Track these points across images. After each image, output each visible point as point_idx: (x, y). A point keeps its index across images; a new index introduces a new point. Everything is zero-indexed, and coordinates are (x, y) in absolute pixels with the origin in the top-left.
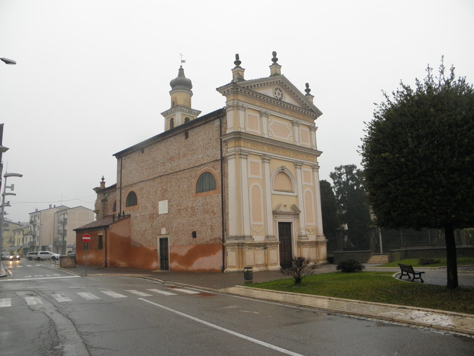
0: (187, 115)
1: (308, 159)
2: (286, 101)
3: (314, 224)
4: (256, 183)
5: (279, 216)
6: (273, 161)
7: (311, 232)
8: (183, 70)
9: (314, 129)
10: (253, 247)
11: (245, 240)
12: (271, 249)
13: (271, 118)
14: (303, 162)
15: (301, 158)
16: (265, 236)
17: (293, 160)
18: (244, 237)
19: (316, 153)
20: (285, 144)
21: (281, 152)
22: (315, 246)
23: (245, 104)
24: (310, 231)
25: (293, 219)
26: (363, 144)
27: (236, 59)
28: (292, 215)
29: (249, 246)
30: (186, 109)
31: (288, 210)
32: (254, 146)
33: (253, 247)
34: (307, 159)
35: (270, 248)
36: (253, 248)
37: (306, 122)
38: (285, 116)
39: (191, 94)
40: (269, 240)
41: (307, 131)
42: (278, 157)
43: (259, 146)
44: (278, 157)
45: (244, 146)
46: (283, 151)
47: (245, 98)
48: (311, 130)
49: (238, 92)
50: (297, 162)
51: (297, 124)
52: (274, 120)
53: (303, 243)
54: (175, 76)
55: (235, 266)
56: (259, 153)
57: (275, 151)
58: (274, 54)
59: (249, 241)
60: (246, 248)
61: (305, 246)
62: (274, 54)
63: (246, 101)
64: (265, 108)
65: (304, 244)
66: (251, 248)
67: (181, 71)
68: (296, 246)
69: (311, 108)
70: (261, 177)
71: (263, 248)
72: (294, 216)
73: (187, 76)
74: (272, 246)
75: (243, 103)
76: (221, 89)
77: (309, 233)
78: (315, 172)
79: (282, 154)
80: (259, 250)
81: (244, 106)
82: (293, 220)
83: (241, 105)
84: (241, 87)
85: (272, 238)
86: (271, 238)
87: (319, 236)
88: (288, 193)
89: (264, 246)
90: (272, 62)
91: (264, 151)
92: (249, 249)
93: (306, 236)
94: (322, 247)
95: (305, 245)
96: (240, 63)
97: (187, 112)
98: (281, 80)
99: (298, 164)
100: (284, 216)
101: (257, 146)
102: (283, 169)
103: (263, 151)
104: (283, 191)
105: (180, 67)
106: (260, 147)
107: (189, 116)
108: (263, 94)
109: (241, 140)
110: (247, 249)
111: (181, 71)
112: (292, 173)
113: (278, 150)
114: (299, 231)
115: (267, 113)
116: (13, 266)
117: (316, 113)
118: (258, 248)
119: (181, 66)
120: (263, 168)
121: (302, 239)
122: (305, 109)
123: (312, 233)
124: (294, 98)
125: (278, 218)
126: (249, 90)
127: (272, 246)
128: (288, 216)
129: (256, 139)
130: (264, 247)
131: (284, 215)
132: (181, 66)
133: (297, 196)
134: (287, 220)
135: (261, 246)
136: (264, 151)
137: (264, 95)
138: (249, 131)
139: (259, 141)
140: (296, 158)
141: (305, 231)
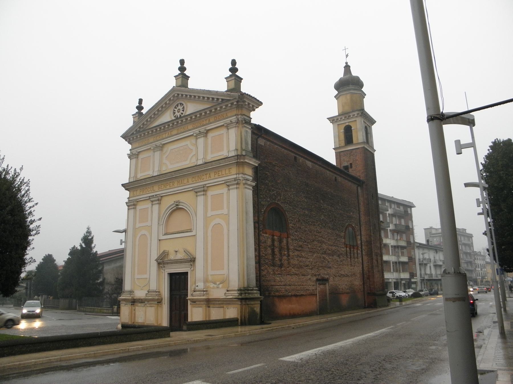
0: (346, 123)
3: (225, 272)
4: (217, 221)
7: (219, 284)
8: (350, 67)
10: (129, 303)
20: (173, 173)
25: (189, 267)
26: (29, 184)
27: (139, 104)
28: (186, 263)
30: (340, 117)
31: (180, 256)
35: (147, 305)
38: (179, 135)
39: (363, 95)
42: (185, 189)
43: (149, 189)
44: (185, 189)
45: (170, 188)
51: (202, 134)
54: (340, 74)
64: (157, 141)
67: (347, 68)
69: (222, 99)
73: (354, 73)
75: (135, 150)
76: (259, 103)
77: (215, 286)
85: (152, 294)
90: (179, 71)
91: (154, 191)
92: (126, 304)
97: (344, 120)
100: (175, 264)
101: (146, 189)
102: (177, 205)
103: (161, 191)
104: (175, 234)
105: (345, 64)
106: (149, 189)
107: (348, 122)
111: (347, 68)
113: (171, 184)
115: (158, 146)
116: (187, 299)
117: (231, 99)
119: (346, 63)
123: (221, 286)
124: (163, 113)
125: (166, 269)
126: (141, 131)
127: (150, 302)
129: (140, 184)
131: (175, 264)
132: (346, 63)
134: (176, 270)
136: (154, 191)
137: (161, 125)
139: (144, 184)
140: (194, 183)
141: (203, 284)
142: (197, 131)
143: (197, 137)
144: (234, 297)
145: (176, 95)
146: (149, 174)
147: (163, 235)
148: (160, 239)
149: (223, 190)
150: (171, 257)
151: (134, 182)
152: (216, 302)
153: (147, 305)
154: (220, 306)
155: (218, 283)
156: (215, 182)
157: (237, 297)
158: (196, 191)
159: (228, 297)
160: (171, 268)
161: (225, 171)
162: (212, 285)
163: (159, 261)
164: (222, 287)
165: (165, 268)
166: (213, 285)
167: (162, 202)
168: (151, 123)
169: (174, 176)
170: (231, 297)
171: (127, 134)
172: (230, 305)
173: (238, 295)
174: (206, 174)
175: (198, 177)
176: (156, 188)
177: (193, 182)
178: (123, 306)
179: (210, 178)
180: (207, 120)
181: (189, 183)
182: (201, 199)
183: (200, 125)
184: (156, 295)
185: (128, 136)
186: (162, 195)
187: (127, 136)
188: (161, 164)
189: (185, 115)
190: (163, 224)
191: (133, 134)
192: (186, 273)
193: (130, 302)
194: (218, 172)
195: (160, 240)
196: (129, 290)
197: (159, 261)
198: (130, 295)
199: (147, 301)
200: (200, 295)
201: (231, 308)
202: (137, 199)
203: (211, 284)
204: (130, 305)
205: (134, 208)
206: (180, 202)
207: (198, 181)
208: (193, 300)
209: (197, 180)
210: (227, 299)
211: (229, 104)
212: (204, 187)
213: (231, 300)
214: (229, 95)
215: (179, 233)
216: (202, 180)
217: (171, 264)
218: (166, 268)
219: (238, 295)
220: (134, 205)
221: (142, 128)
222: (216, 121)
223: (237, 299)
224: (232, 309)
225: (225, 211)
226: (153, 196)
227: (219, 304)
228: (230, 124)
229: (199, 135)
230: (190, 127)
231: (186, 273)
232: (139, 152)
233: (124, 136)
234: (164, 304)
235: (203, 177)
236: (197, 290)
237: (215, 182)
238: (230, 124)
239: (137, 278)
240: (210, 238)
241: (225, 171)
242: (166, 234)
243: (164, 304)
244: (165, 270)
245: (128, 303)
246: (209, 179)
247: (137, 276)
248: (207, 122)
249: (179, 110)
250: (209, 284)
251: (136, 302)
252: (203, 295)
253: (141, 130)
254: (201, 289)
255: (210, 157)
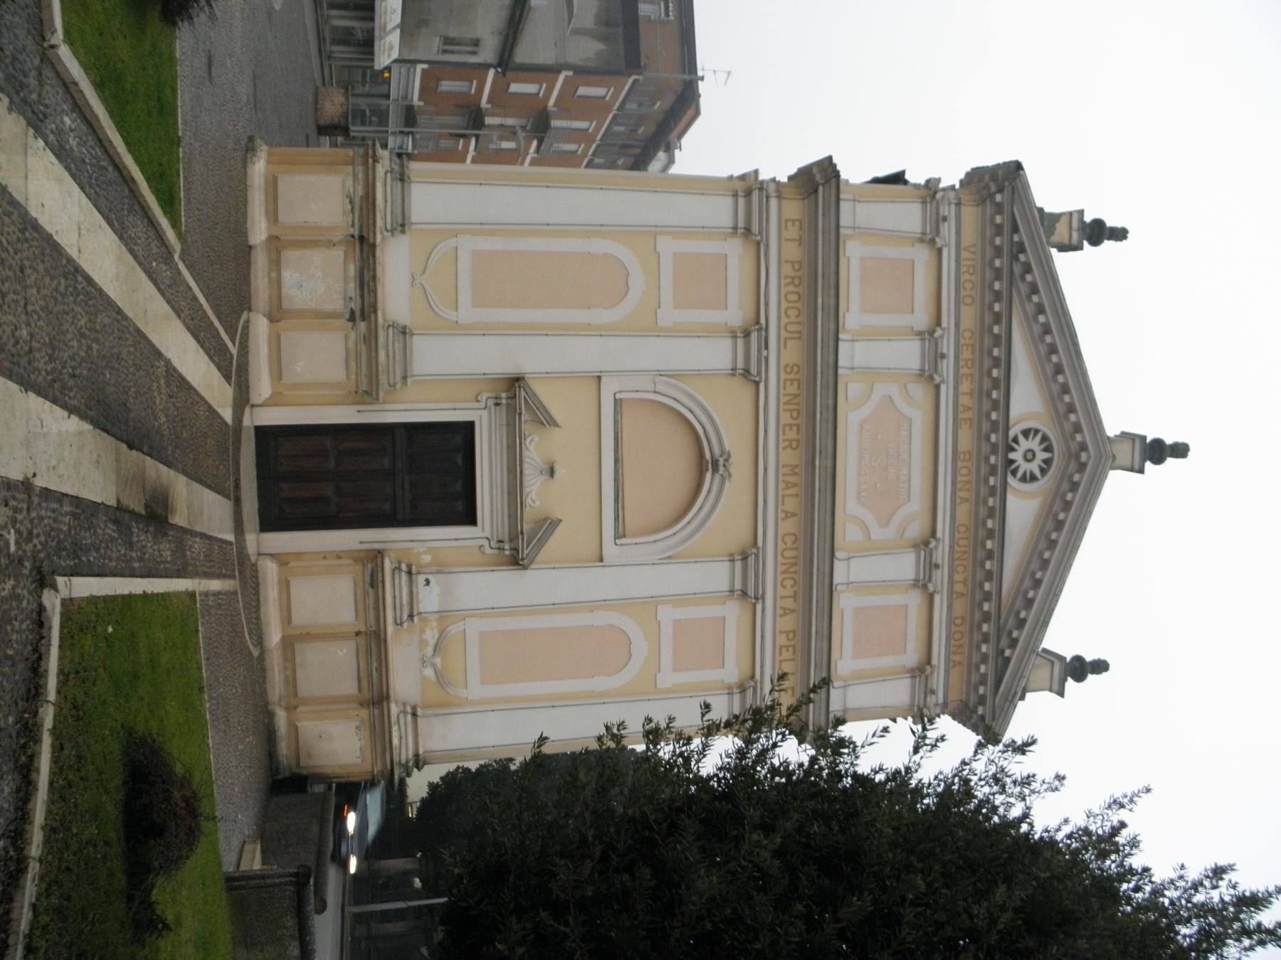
1: (781, 647)
2: (1013, 502)
3: (476, 690)
5: (501, 425)
6: (740, 393)
7: (434, 665)
9: (922, 697)
10: (356, 222)
11: (389, 174)
12: (346, 338)
13: (914, 601)
14: (763, 598)
15: (784, 475)
16: (408, 323)
17: (765, 533)
18: (402, 180)
19: (817, 632)
21: (792, 389)
22: (366, 694)
23: (949, 225)
24: (438, 660)
29: (362, 197)
32: (793, 278)
33: (356, 222)
34: (782, 640)
35: (353, 334)
36: (353, 225)
37: (943, 642)
40: (391, 329)
41: (905, 652)
46: (797, 466)
47: (974, 245)
48: (913, 677)
49: (988, 202)
50: (757, 556)
52: (919, 420)
53: (375, 582)
55: (276, 220)
56: (767, 304)
57: (791, 411)
58: (1180, 450)
59: (386, 201)
60: (355, 175)
61: (360, 592)
62: (1180, 450)
63: (965, 249)
65: (371, 591)
66: (353, 209)
68: (361, 543)
69: (1008, 660)
70: (669, 315)
71: (353, 305)
72: (506, 538)
74: (363, 349)
78: (726, 697)
79: (783, 460)
80: (346, 282)
81: (937, 575)
82: (487, 534)
83: (941, 210)
84: (1012, 207)
86: (397, 345)
87: (414, 715)
88: (612, 497)
89: (362, 310)
91: (782, 343)
93: (411, 616)
94: (358, 728)
95: (365, 593)
96: (1095, 242)
98: (1089, 457)
99: (751, 560)
106: (793, 313)
108: (1013, 357)
109: (806, 201)
110: (349, 183)
112: (708, 525)
114: (434, 569)
118: (355, 277)
120: (706, 332)
121: (396, 572)
122: (999, 631)
123: (429, 672)
125: (490, 414)
128: (502, 493)
130: (358, 314)
133: (601, 560)
134: (486, 480)
135: (362, 296)
136: (782, 343)
138: (849, 258)
139: (820, 300)
142: (948, 347)
143: (928, 335)
144: (395, 752)
145: (1084, 457)
146: (848, 311)
147: (618, 396)
148: (603, 379)
149: (735, 313)
150: (532, 440)
151: (838, 227)
152: (374, 658)
153: (353, 334)
154: (362, 674)
155: (438, 660)
156: (763, 636)
157: (396, 759)
158: (747, 556)
159: (395, 728)
160: (493, 433)
161: (789, 660)
162: (431, 636)
163: (523, 393)
164: (424, 680)
165: (493, 407)
166: (432, 642)
167: (738, 382)
168: (1030, 321)
169: (817, 463)
170: (395, 741)
171: (1021, 198)
172: (368, 732)
173: (403, 761)
174: (795, 597)
175: (794, 560)
176: (794, 252)
177: (786, 312)
178: (344, 185)
179: (782, 612)
180: (965, 586)
181: (781, 616)
182: (718, 576)
183: (956, 556)
184: (391, 382)
185: (1013, 201)
186: (762, 386)
187: (1016, 196)
188: (872, 374)
189: (1009, 490)
190: (655, 392)
191: (1015, 229)
192: (469, 518)
193: (361, 228)
194: (798, 425)
195: (599, 378)
196: (409, 218)
197: (523, 393)
198: (389, 227)
199: (369, 329)
200: (398, 606)
201: (360, 739)
202: (767, 246)
203: (436, 630)
204: (351, 231)
205: (735, 228)
206: (723, 479)
207: (780, 559)
208: (380, 585)
209: (784, 557)
210: (390, 727)
211: (986, 691)
212: (757, 598)
213: (387, 740)
214: (1010, 698)
215: (615, 480)
216: (779, 580)
217: (509, 490)
218: (493, 412)
219: (403, 761)
220: (748, 230)
221: (1023, 279)
222: (951, 620)
223: (389, 767)
224: (358, 744)
225: (669, 315)
226: (767, 348)
227: (370, 675)
228: (926, 686)
229: (928, 558)
230: (963, 512)
231: (469, 518)
232: (940, 251)
233: (1019, 185)
234: (359, 411)
235: (789, 583)
236: (408, 341)
237: (763, 636)
238: (926, 686)
239: (457, 248)
240: (585, 619)
241: (789, 660)
242: (618, 403)
243: (359, 411)
244: (485, 408)
245: (357, 215)
246: (780, 511)
247: (467, 245)
248: (959, 588)
249: (1030, 456)
250: (435, 624)
251: (362, 250)
252: (399, 622)
253: (1017, 269)
254: (418, 598)
255: (854, 252)
